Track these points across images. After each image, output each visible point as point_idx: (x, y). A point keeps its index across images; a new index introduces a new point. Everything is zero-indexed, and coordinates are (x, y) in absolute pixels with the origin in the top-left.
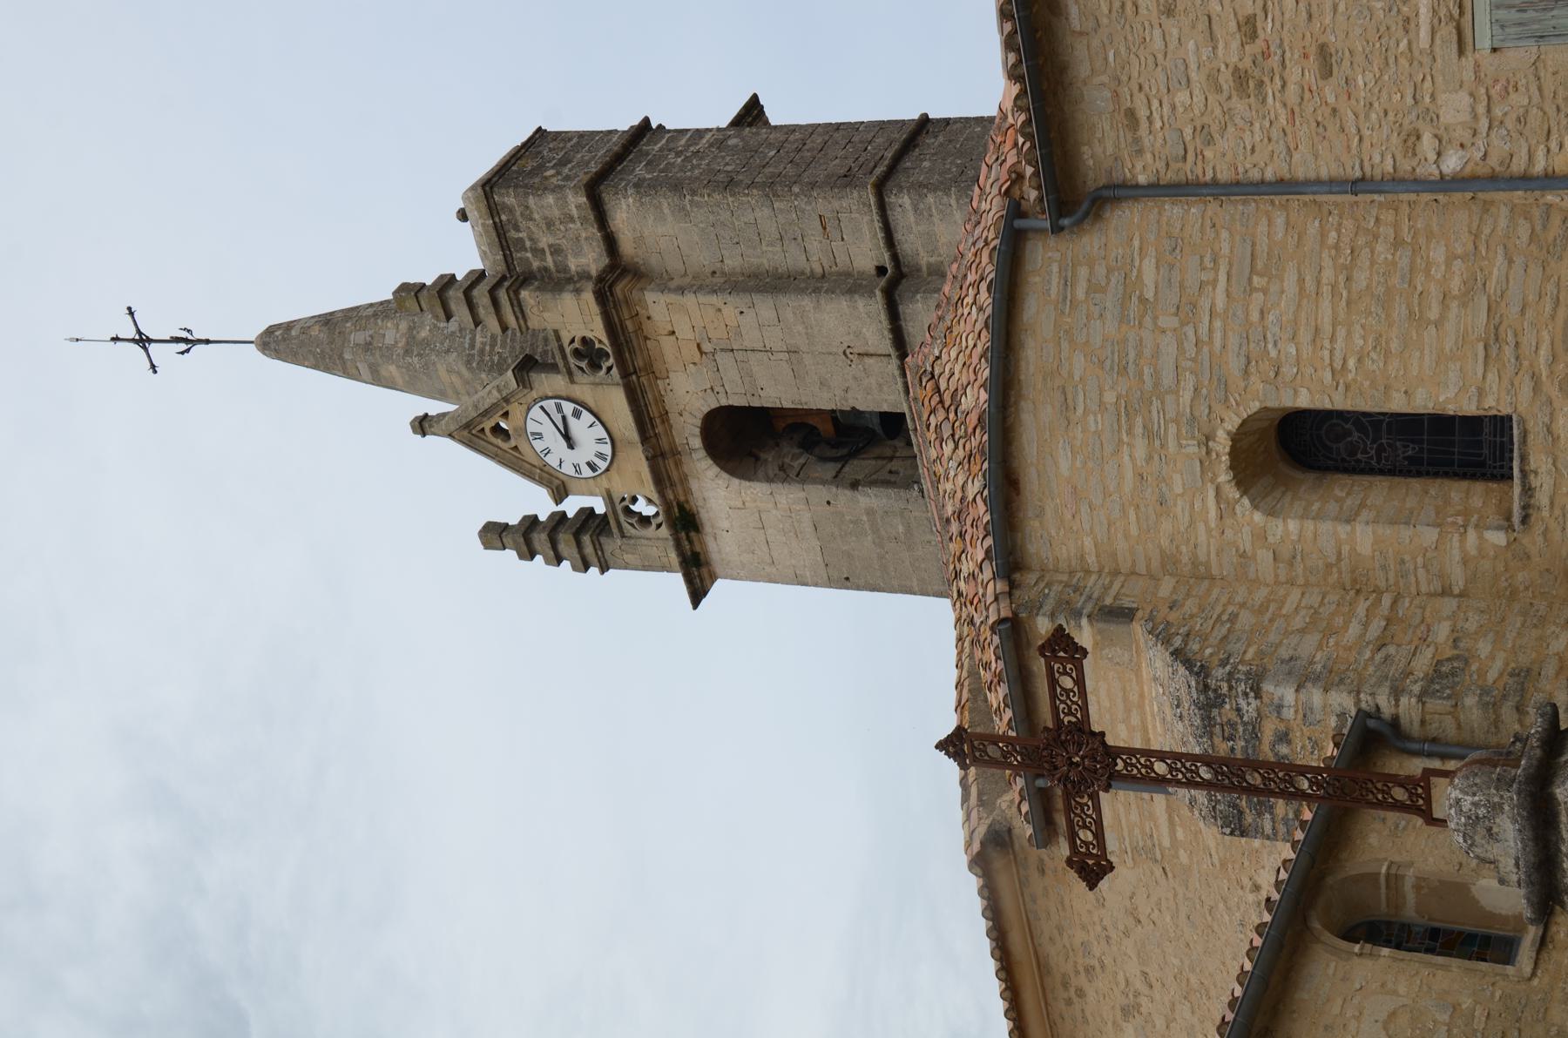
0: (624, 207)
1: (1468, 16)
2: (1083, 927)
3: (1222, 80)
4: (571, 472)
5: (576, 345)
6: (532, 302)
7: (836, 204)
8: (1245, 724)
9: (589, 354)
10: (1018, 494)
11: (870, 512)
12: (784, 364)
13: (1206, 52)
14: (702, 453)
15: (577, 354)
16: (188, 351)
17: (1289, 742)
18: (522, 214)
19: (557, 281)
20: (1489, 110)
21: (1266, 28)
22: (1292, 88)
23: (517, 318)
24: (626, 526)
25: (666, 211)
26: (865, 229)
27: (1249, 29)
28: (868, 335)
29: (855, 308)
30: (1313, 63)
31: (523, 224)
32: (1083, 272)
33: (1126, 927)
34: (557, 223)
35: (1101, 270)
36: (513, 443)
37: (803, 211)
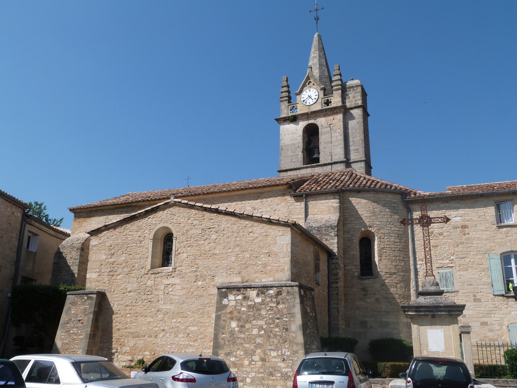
1: (444, 268)
2: (271, 201)
4: (302, 97)
5: (330, 100)
6: (339, 92)
7: (361, 152)
8: (328, 233)
9: (328, 103)
10: (357, 193)
11: (297, 155)
13: (436, 227)
14: (308, 123)
15: (328, 100)
16: (315, 19)
17: (326, 241)
19: (344, 97)
21: (441, 237)
24: (291, 106)
25: (358, 120)
27: (441, 234)
28: (336, 157)
29: (341, 155)
31: (354, 92)
32: (396, 205)
35: (397, 208)
36: (308, 85)
37: (359, 146)
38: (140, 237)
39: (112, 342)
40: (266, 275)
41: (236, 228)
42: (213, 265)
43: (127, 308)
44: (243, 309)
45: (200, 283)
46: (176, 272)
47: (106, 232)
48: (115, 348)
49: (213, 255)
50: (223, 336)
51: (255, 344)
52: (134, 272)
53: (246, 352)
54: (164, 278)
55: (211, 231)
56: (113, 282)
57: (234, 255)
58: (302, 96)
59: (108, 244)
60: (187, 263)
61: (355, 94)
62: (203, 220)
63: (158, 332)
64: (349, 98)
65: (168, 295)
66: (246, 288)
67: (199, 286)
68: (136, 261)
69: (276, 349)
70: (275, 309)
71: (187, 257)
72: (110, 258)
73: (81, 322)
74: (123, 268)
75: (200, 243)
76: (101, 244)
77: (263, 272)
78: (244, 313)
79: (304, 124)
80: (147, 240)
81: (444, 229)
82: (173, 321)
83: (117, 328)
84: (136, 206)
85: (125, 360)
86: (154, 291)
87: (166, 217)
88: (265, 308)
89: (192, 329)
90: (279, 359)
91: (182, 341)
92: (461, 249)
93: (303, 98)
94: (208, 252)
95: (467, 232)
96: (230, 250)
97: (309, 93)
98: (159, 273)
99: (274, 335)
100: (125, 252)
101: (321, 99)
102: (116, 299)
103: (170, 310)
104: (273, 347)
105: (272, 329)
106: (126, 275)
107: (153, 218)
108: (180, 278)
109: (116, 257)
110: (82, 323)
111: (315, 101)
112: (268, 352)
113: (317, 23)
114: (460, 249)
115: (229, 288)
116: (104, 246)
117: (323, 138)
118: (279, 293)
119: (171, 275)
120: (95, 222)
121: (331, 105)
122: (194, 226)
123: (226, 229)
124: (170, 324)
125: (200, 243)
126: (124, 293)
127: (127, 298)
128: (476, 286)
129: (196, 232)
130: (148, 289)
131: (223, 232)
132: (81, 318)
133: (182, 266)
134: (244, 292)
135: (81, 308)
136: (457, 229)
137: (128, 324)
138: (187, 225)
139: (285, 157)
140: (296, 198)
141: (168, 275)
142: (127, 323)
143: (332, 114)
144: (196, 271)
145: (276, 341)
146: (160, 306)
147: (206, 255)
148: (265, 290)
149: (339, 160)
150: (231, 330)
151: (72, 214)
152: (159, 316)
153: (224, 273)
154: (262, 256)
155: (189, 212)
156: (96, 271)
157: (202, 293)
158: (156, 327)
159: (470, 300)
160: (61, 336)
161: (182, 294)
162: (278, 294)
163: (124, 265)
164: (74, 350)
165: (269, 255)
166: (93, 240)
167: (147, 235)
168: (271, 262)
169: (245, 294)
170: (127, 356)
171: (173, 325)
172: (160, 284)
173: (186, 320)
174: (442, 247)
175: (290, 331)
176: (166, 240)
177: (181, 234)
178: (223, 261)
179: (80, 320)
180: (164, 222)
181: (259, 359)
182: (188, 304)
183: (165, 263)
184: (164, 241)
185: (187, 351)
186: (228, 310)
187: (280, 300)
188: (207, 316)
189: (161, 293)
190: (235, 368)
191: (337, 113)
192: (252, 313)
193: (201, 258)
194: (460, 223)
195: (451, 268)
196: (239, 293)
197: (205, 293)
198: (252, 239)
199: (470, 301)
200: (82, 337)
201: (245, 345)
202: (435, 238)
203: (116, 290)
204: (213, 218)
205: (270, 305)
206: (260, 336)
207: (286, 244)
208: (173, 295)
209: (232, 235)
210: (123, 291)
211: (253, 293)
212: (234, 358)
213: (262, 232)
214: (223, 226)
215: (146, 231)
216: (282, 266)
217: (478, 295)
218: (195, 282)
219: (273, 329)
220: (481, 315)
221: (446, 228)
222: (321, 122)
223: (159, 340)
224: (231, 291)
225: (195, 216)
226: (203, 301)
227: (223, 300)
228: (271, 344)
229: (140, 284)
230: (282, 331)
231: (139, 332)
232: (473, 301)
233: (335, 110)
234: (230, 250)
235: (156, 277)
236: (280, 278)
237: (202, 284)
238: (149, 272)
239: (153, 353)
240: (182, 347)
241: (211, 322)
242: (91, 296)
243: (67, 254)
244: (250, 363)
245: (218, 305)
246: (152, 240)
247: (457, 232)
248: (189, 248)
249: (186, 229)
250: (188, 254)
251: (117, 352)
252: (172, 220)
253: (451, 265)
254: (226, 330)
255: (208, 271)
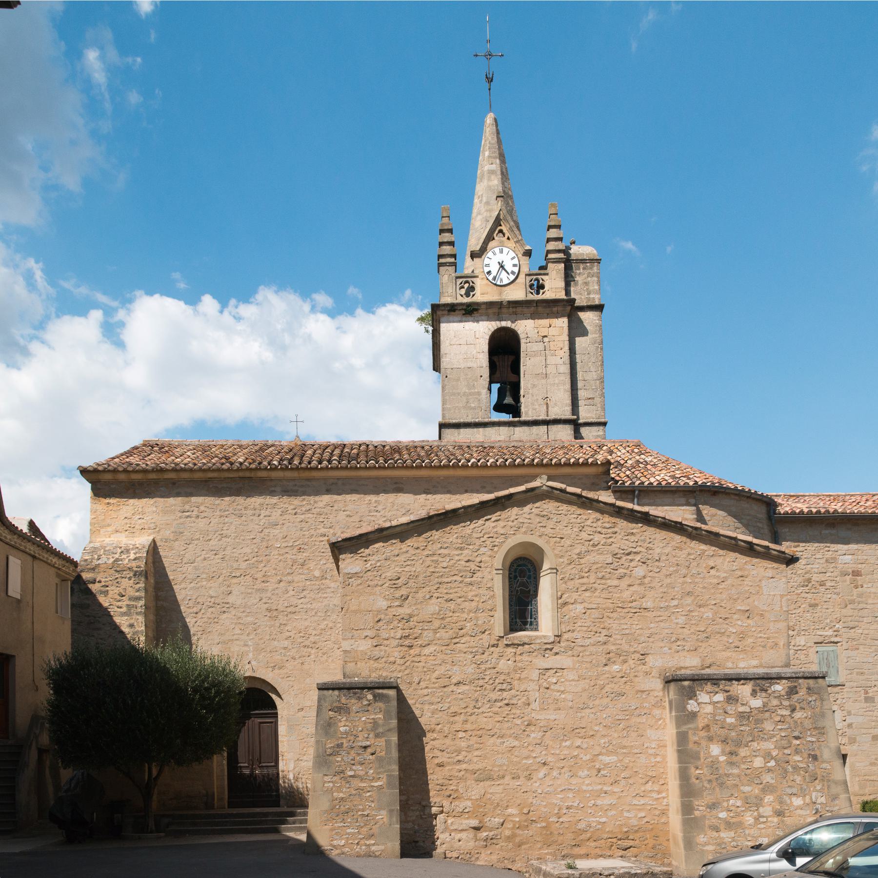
0: (595, 318)
3: (808, 575)
6: (560, 267)
11: (479, 393)
12: (541, 371)
14: (499, 326)
18: (590, 273)
19: (569, 279)
20: (800, 650)
21: (822, 589)
22: (807, 595)
23: (554, 259)
24: (461, 280)
26: (589, 415)
27: (822, 584)
30: (813, 602)
31: (586, 272)
33: (552, 519)
34: (587, 287)
36: (496, 238)
37: (596, 392)
38: (468, 561)
39: (428, 791)
40: (746, 654)
41: (684, 556)
42: (641, 631)
43: (456, 718)
44: (729, 720)
45: (616, 667)
46: (562, 644)
47: (381, 544)
48: (437, 805)
49: (640, 611)
50: (697, 772)
51: (761, 786)
52: (463, 640)
53: (746, 801)
54: (536, 656)
55: (631, 560)
56: (413, 661)
57: (683, 613)
58: (487, 261)
59: (388, 574)
60: (586, 625)
61: (588, 276)
62: (614, 535)
63: (533, 768)
64: (576, 284)
65: (548, 691)
66: (730, 679)
67: (615, 674)
68: (465, 616)
69: (802, 793)
70: (788, 719)
71: (585, 613)
72: (400, 606)
73: (369, 750)
74: (435, 631)
75: (609, 583)
76: (369, 573)
77: (740, 649)
78: (732, 728)
79: (490, 327)
80: (488, 570)
81: (828, 575)
82: (564, 744)
83: (436, 761)
84: (263, 480)
85: (464, 827)
86: (516, 683)
87: (529, 521)
88: (771, 718)
89: (606, 759)
90: (808, 811)
91: (588, 785)
92: (850, 612)
93: (487, 265)
94: (630, 605)
95: (860, 583)
96: (675, 602)
97: (499, 257)
98: (524, 644)
99: (794, 768)
100: (436, 595)
101: (524, 276)
102: (426, 698)
103: (556, 722)
104: (794, 791)
105: (788, 756)
106: (445, 647)
107: (497, 521)
108: (573, 656)
109: (415, 604)
110: (372, 754)
111: (512, 277)
112: (786, 798)
113: (490, 89)
114: (848, 611)
115: (698, 680)
116: (378, 578)
117: (529, 365)
118: (792, 691)
119: (551, 650)
120: (154, 509)
121: (543, 293)
122: (594, 545)
123: (664, 558)
124: (557, 752)
125: (609, 583)
126: (445, 687)
127: (454, 696)
128: (868, 677)
129: (601, 559)
130: (502, 677)
131: (657, 563)
132: (368, 743)
133: (573, 631)
134: (727, 688)
135: (363, 719)
136: (846, 576)
137: (463, 753)
138: (578, 542)
139: (454, 394)
140: (618, 494)
141: (546, 649)
142: (459, 752)
143: (548, 314)
144: (605, 643)
145: (798, 779)
146: (533, 715)
147: (626, 610)
148: (768, 685)
149: (563, 417)
150: (712, 761)
151: (86, 487)
152: (533, 735)
153: (666, 649)
154: (736, 616)
155: (580, 515)
156: (366, 634)
157: (622, 687)
158: (527, 758)
159: (859, 699)
160: (325, 782)
161: (579, 689)
162: (791, 693)
163: (437, 623)
164: (366, 813)
165: (748, 613)
166: (348, 561)
167: (484, 558)
168: (753, 629)
169: (729, 691)
170: (468, 818)
171: (565, 752)
172: (529, 667)
173: (592, 743)
174: (824, 607)
175: (820, 760)
176: (515, 572)
177: (566, 562)
178: (662, 625)
179: (365, 747)
180: (525, 533)
181: (771, 813)
182: (593, 710)
183: (516, 622)
184: (510, 574)
185: (599, 802)
186: (701, 722)
187: (796, 704)
188: (636, 734)
189: (532, 686)
190: (731, 831)
191: (557, 315)
192: (748, 728)
193: (615, 615)
194: (851, 566)
195: (835, 645)
196: (717, 690)
197: (627, 687)
198: (716, 581)
199: (860, 701)
200: (380, 783)
201: (742, 788)
202: (813, 591)
203: (425, 680)
204: (634, 531)
205: (780, 712)
206: (769, 770)
207: (779, 596)
208: (558, 691)
209: (677, 571)
210: (443, 682)
211: (744, 690)
212: (724, 813)
213: (734, 568)
214: (658, 550)
215: (483, 550)
216: (773, 638)
217: (870, 691)
218: (606, 665)
219: (790, 757)
220: (873, 724)
221: (830, 574)
222: (525, 328)
223: (537, 784)
224: (702, 685)
225: (594, 525)
226: (626, 704)
227: (688, 704)
228: (790, 784)
229: (481, 666)
230: (806, 760)
231: (490, 768)
232: (863, 701)
233: (555, 306)
234: (675, 602)
235: (518, 653)
236: (772, 661)
237: (621, 670)
238: (500, 642)
239: (525, 811)
240: (588, 795)
241: (645, 746)
242: (382, 694)
243: (107, 584)
244: (757, 819)
245: (678, 712)
246: (501, 572)
247: (845, 581)
248: (587, 594)
249: (577, 551)
250: (586, 605)
251: (442, 812)
252: (542, 529)
253: (836, 639)
254: (702, 760)
255: (632, 644)
